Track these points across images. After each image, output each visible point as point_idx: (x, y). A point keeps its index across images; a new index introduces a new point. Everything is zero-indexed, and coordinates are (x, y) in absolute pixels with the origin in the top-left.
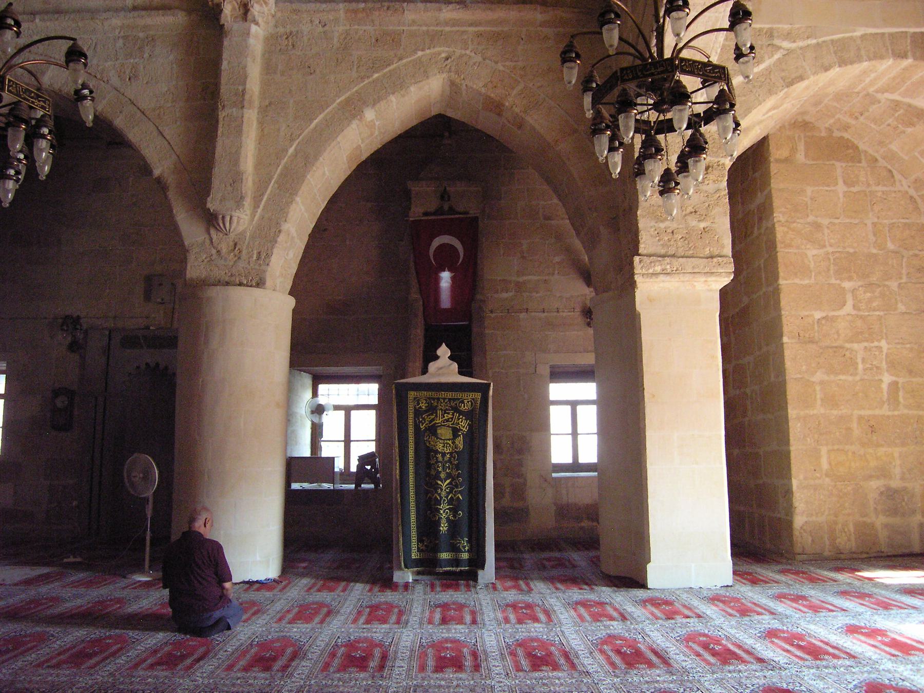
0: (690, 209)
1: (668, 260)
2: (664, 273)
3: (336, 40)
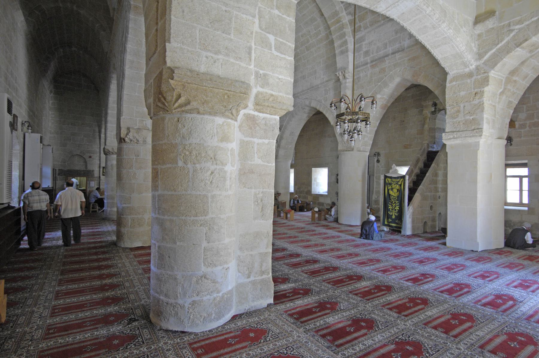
0: (467, 112)
1: (455, 133)
2: (454, 138)
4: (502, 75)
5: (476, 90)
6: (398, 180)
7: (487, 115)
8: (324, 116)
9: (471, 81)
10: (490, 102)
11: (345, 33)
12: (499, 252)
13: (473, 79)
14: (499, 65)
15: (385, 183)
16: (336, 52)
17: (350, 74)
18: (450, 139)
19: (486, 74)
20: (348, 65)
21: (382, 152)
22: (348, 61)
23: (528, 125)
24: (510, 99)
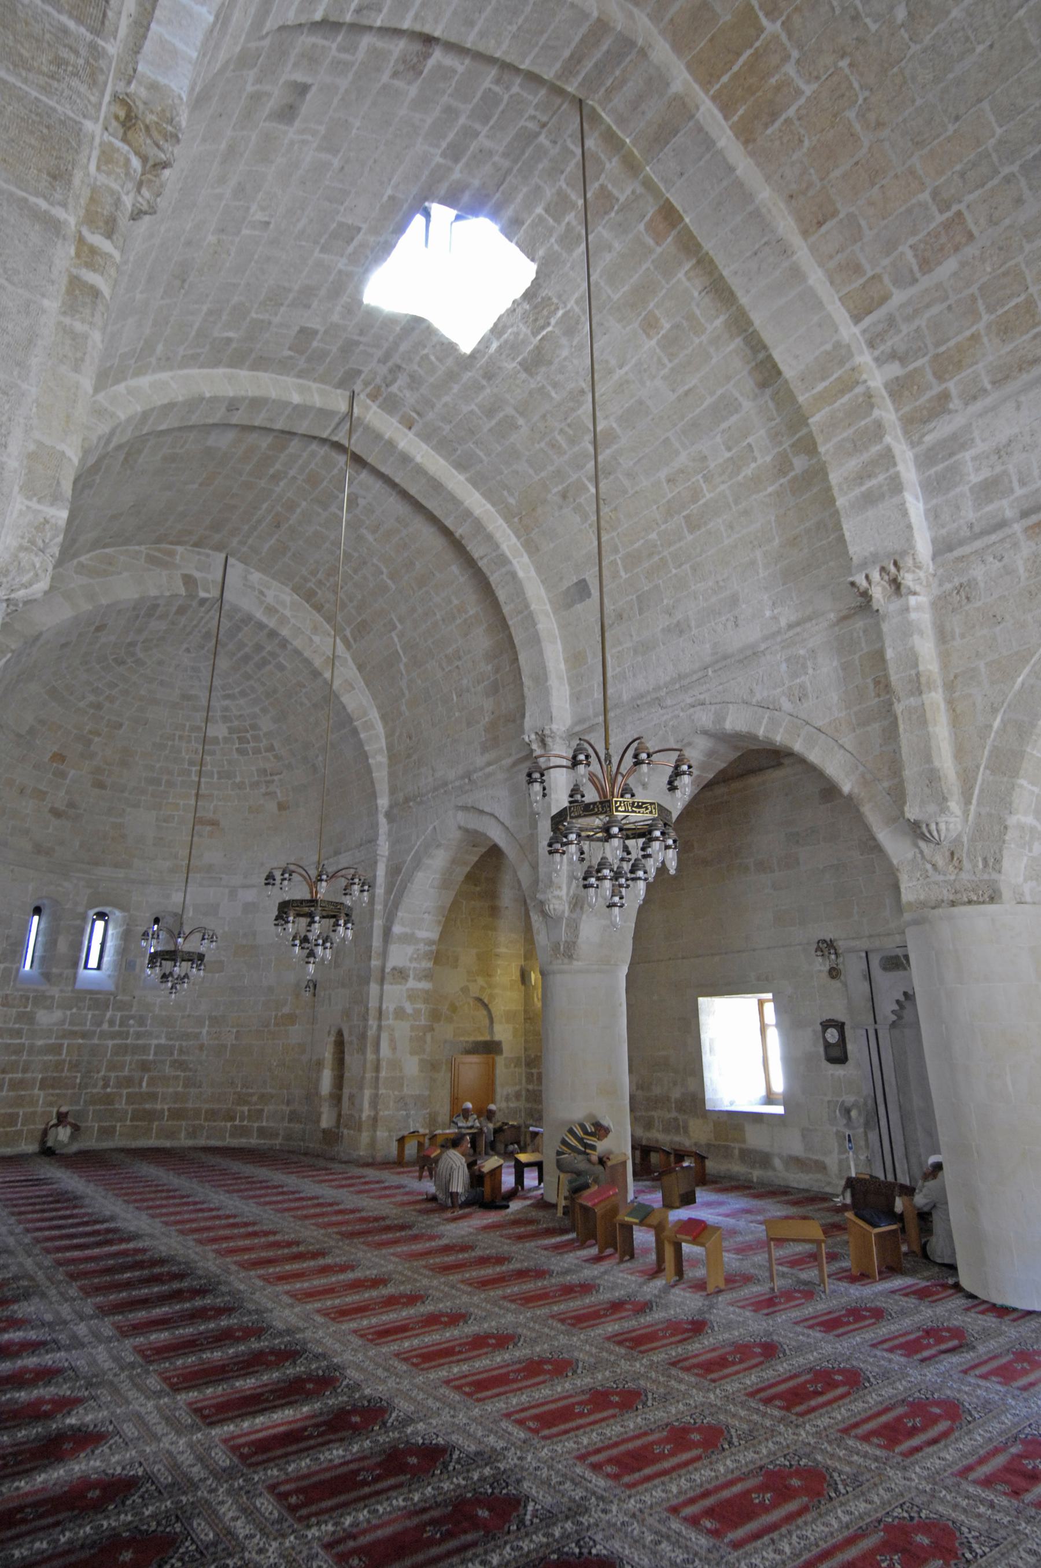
3: (1021, 570)
8: (802, 761)
16: (841, 502)
17: (922, 574)
20: (910, 539)
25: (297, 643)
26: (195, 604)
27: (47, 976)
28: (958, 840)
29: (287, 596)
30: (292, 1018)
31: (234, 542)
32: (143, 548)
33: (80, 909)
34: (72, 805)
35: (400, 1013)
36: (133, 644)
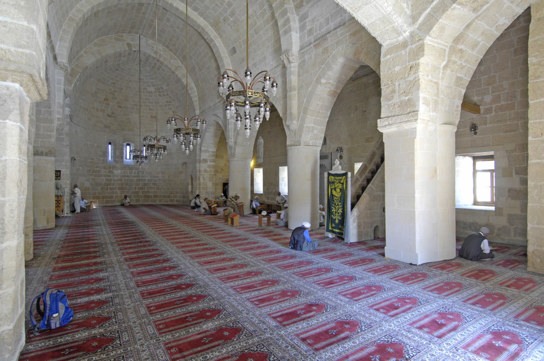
0: (402, 91)
1: (390, 118)
2: (389, 125)
4: (443, 43)
5: (411, 63)
6: (341, 178)
7: (424, 94)
9: (406, 51)
10: (430, 77)
11: (286, 9)
12: (444, 265)
13: (407, 50)
14: (435, 29)
15: (329, 182)
17: (294, 57)
18: (385, 126)
19: (421, 42)
21: (345, 147)
22: (294, 41)
23: (494, 109)
24: (458, 75)
25: (166, 63)
26: (132, 52)
27: (115, 161)
28: (296, 130)
29: (161, 47)
30: (182, 172)
31: (140, 31)
32: (113, 35)
33: (121, 143)
34: (113, 113)
35: (206, 171)
36: (118, 64)
